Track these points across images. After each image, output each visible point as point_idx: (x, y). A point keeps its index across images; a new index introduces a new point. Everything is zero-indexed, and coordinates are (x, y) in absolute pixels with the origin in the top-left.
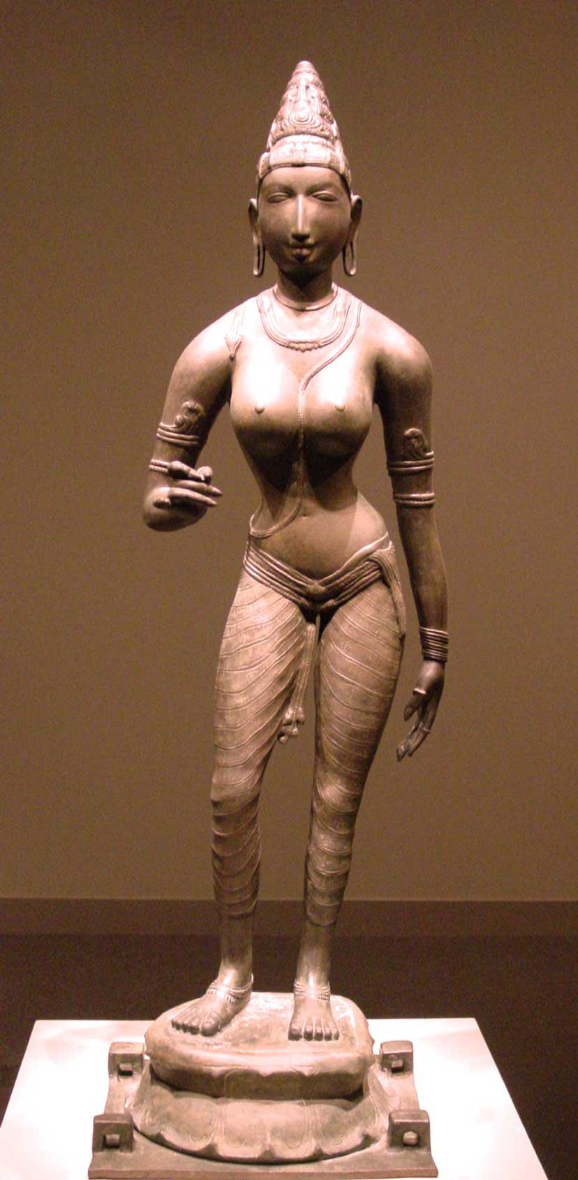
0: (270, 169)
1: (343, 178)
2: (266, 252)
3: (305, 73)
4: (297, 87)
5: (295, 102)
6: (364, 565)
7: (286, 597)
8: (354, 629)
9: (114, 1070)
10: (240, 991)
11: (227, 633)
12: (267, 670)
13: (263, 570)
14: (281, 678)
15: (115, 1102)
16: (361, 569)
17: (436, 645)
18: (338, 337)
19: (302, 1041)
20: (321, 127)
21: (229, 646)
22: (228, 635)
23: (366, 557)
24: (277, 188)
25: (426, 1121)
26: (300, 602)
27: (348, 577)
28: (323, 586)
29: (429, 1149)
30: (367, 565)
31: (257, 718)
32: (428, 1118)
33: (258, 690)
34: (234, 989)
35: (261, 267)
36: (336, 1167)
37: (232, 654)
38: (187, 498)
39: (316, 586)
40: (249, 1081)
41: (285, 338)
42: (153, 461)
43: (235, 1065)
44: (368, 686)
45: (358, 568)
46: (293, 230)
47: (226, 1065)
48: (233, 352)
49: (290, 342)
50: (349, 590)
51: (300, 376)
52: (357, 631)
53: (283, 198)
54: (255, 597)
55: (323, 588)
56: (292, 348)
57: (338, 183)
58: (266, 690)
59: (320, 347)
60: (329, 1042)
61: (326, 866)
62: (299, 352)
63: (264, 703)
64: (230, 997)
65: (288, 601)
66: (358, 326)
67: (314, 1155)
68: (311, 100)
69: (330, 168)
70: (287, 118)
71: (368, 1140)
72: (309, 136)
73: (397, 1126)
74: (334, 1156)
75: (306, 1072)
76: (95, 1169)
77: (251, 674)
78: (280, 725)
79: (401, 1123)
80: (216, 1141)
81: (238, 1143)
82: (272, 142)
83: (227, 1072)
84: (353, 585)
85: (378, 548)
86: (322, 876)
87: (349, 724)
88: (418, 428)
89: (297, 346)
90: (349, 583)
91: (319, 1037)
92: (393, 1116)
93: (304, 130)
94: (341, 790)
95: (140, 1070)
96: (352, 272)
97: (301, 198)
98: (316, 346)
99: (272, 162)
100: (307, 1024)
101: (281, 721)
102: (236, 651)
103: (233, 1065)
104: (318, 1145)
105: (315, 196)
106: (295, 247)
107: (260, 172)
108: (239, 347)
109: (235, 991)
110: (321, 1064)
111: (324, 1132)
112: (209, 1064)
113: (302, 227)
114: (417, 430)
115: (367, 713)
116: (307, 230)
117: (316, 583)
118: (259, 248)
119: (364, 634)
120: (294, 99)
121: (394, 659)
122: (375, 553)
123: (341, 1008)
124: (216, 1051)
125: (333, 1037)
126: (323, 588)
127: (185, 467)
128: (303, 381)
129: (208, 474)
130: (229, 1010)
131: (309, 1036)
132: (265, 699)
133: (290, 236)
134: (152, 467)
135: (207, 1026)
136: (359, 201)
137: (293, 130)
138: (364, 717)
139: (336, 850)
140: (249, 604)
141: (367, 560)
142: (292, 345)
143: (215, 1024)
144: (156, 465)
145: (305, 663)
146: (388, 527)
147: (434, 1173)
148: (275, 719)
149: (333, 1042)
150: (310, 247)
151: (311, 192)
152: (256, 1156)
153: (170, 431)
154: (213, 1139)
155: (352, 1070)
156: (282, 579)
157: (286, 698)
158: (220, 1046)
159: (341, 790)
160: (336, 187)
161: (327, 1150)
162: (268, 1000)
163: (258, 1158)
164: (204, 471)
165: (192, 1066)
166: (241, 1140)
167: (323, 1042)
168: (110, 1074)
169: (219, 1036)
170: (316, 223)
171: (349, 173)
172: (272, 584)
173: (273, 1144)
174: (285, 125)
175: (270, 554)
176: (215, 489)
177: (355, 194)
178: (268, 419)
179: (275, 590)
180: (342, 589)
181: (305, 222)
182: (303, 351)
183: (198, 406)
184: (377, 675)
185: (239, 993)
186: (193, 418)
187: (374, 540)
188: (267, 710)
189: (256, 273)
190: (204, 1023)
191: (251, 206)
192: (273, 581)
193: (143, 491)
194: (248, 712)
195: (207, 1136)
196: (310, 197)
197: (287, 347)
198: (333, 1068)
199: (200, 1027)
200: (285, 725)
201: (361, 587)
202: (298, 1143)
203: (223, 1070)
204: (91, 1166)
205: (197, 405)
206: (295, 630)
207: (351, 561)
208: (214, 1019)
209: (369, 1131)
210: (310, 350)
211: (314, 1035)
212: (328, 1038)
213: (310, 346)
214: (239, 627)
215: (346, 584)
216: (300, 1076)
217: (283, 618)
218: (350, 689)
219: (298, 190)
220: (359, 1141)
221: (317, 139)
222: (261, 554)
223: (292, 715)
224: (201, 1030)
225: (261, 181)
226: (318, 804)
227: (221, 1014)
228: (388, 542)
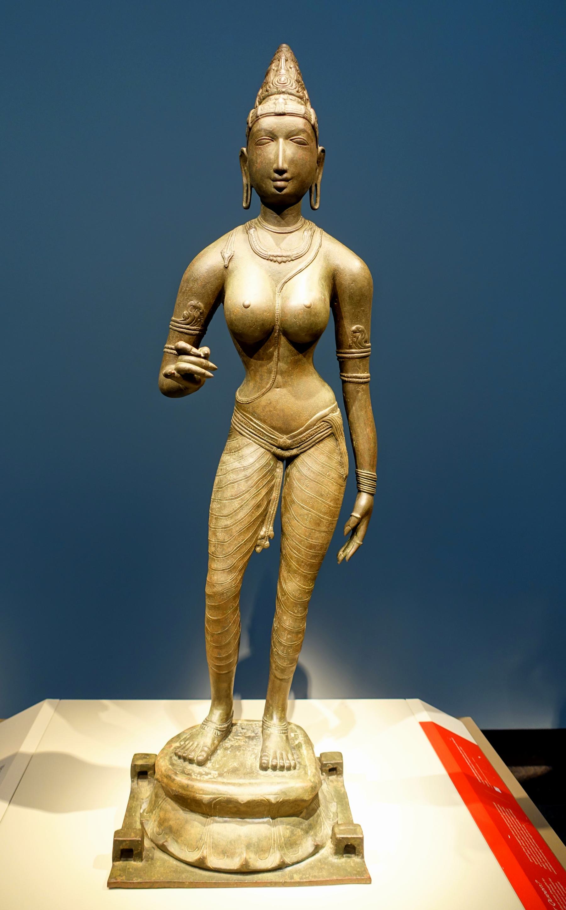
0: (257, 118)
1: (313, 127)
2: (253, 189)
3: (285, 52)
4: (279, 60)
5: (277, 71)
6: (320, 425)
7: (262, 447)
8: (312, 471)
9: (135, 776)
10: (224, 726)
11: (219, 473)
12: (248, 501)
13: (254, 432)
14: (258, 506)
15: (134, 805)
16: (318, 428)
17: (368, 483)
18: (301, 257)
19: (270, 771)
20: (297, 89)
21: (221, 481)
22: (219, 474)
23: (322, 419)
24: (263, 133)
25: (361, 836)
26: (272, 451)
27: (309, 433)
28: (290, 440)
29: (363, 857)
30: (322, 425)
31: (239, 535)
32: (362, 833)
33: (241, 515)
34: (220, 725)
35: (249, 201)
36: (295, 876)
37: (222, 488)
38: (189, 370)
39: (284, 439)
40: (230, 806)
41: (266, 253)
42: (167, 345)
43: (221, 794)
44: (321, 512)
45: (315, 427)
46: (275, 166)
47: (214, 794)
48: (226, 263)
49: (270, 256)
50: (309, 443)
51: (277, 282)
52: (314, 473)
53: (268, 141)
54: (239, 446)
55: (289, 441)
56: (271, 261)
57: (310, 131)
58: (246, 515)
59: (292, 260)
60: (289, 772)
61: (287, 638)
62: (277, 264)
63: (246, 523)
64: (217, 731)
65: (263, 450)
66: (320, 246)
67: (279, 865)
68: (290, 69)
69: (304, 118)
70: (271, 82)
71: (317, 848)
72: (288, 95)
73: (340, 840)
74: (293, 864)
75: (273, 799)
76: (113, 880)
77: (236, 504)
78: (257, 539)
79: (342, 838)
80: (205, 854)
81: (222, 855)
82: (259, 102)
83: (215, 799)
84: (312, 439)
85: (331, 413)
86: (285, 646)
87: (307, 540)
88: (361, 325)
89: (275, 259)
90: (309, 437)
91: (282, 768)
92: (336, 830)
93: (284, 90)
94: (300, 586)
95: (153, 775)
96: (316, 207)
97: (281, 140)
98: (290, 259)
99: (259, 113)
100: (273, 759)
101: (258, 536)
102: (225, 486)
103: (218, 794)
104: (282, 857)
105: (291, 140)
106: (275, 180)
107: (250, 122)
108: (231, 259)
109: (221, 726)
110: (284, 793)
111: (285, 844)
112: (201, 792)
113: (282, 164)
114: (361, 326)
115: (320, 532)
116: (286, 166)
117: (285, 437)
118: (247, 185)
119: (319, 475)
120: (276, 69)
121: (340, 493)
122: (328, 416)
123: (295, 735)
124: (207, 781)
125: (292, 768)
126: (289, 441)
127: (188, 346)
128: (279, 286)
129: (206, 352)
130: (216, 742)
131: (274, 768)
132: (248, 520)
133: (272, 171)
134: (166, 350)
135: (200, 758)
136: (323, 151)
137: (276, 90)
138: (317, 534)
139: (294, 628)
140: (235, 452)
141: (323, 421)
142: (271, 258)
143: (206, 757)
144: (168, 348)
145: (275, 494)
146: (337, 399)
147: (368, 880)
148: (252, 536)
149: (292, 772)
150: (286, 180)
151: (289, 136)
152: (236, 868)
153: (178, 323)
154: (203, 852)
155: (307, 797)
156: (260, 434)
157: (261, 520)
158: (209, 776)
159: (300, 586)
160: (309, 134)
161: (288, 860)
162: (243, 727)
163: (236, 870)
164: (204, 350)
165: (188, 793)
166: (225, 853)
167: (285, 773)
168: (132, 778)
169: (209, 764)
170: (292, 162)
171: (317, 125)
172: (252, 437)
173: (248, 857)
174: (269, 87)
175: (251, 416)
176: (211, 364)
177: (320, 146)
178: (252, 312)
179: (255, 442)
180: (303, 442)
181: (284, 160)
182: (280, 263)
183: (201, 304)
184: (328, 504)
185: (224, 728)
186: (196, 314)
187: (327, 407)
188: (248, 529)
189: (244, 205)
190: (198, 756)
191: (242, 152)
192: (253, 435)
193: (159, 366)
194: (234, 531)
195: (198, 848)
196: (288, 141)
197: (268, 260)
198: (292, 796)
199: (195, 759)
200: (260, 539)
201: (318, 441)
202: (266, 855)
203: (211, 798)
204: (110, 877)
205: (199, 303)
206: (269, 471)
207: (311, 422)
208: (206, 752)
209: (318, 840)
210: (285, 262)
211: (278, 767)
212: (289, 769)
213: (285, 259)
214: (228, 469)
215: (307, 439)
216: (269, 801)
217: (260, 462)
218: (307, 515)
219: (279, 134)
220: (311, 849)
221: (294, 98)
222: (243, 414)
223: (265, 532)
224: (196, 761)
225: (250, 129)
226: (282, 595)
227: (210, 747)
228: (337, 408)
